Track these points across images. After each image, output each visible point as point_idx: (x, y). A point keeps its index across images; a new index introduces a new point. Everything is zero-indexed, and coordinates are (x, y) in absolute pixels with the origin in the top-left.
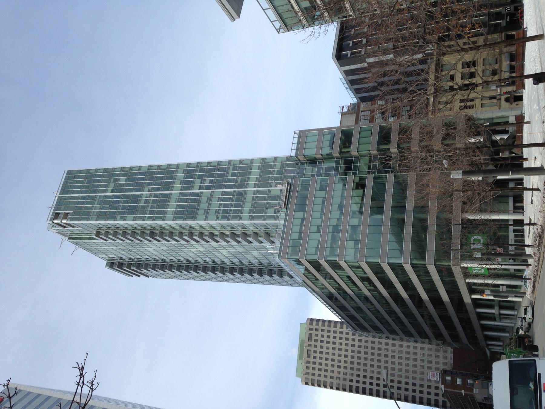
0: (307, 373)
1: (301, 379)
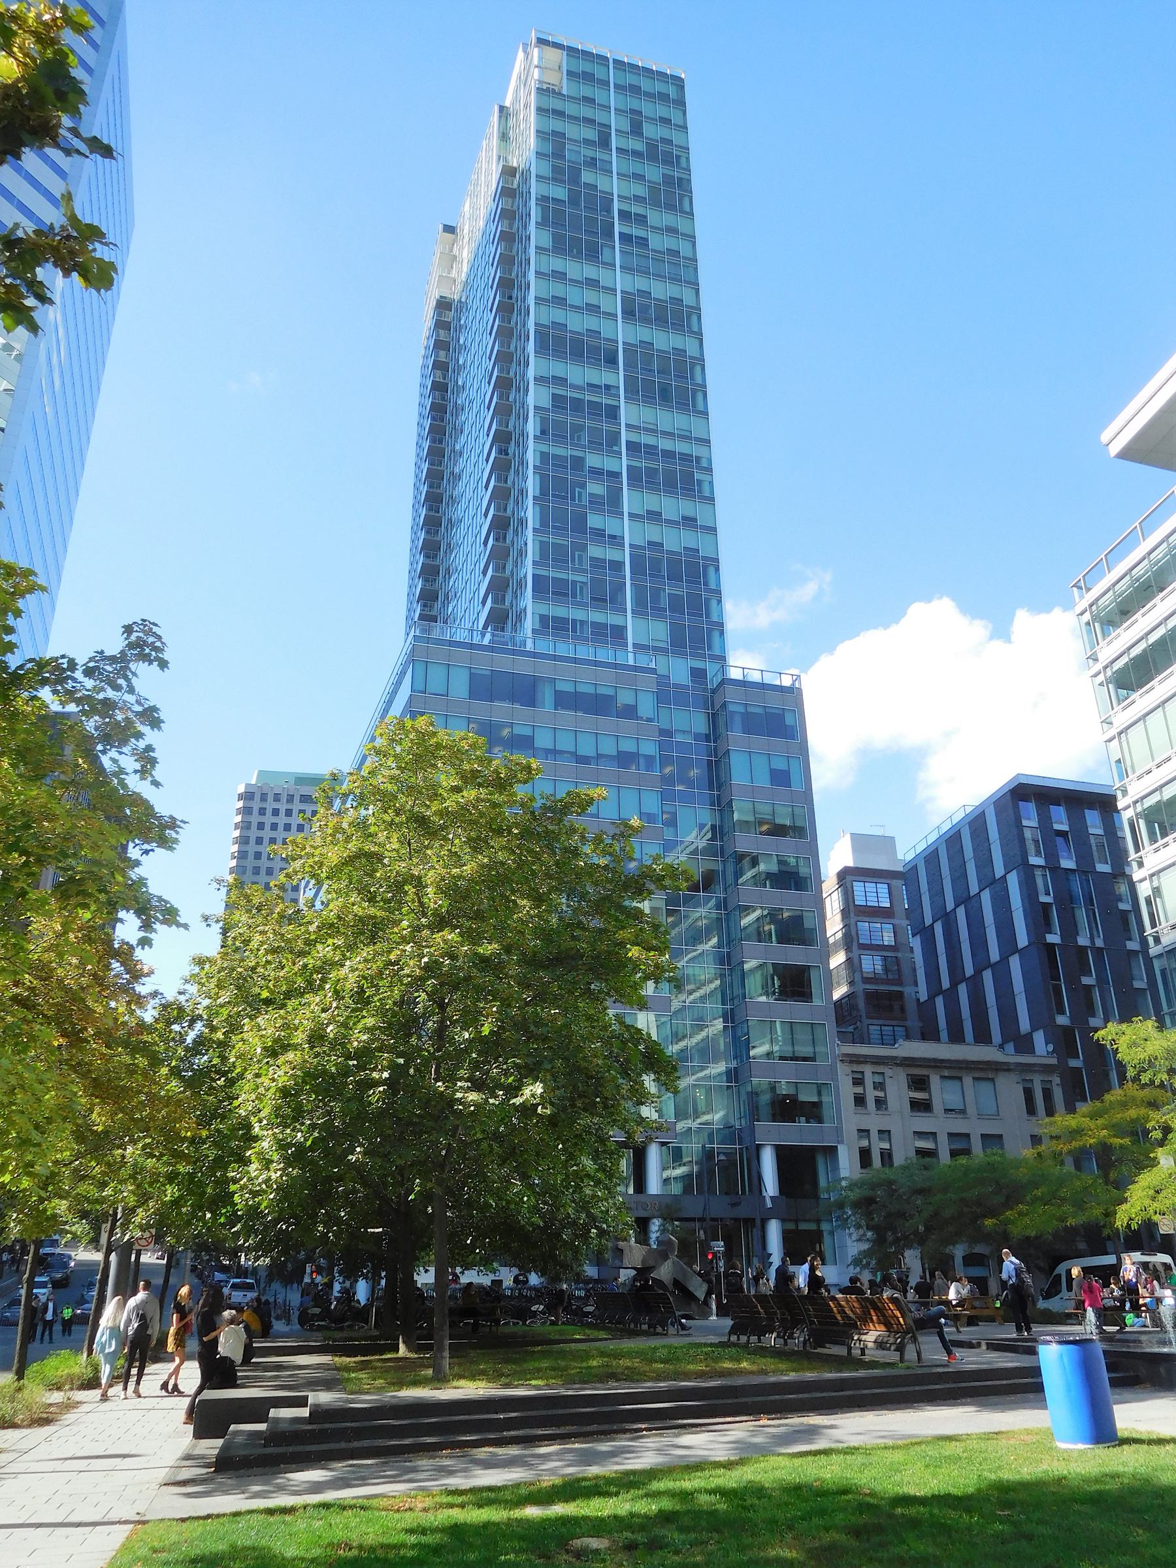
1: (253, 782)
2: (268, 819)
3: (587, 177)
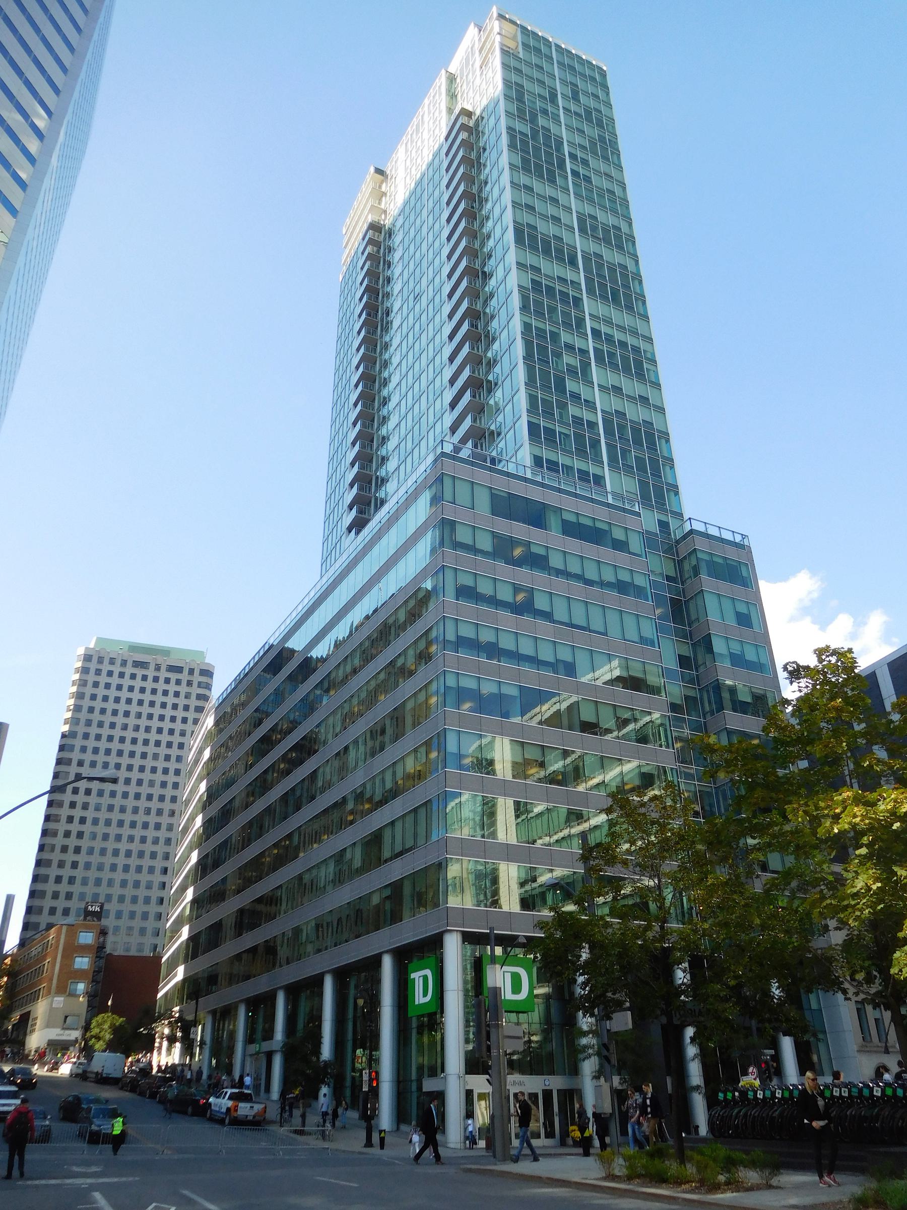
1: (92, 646)
2: (103, 679)
3: (541, 121)
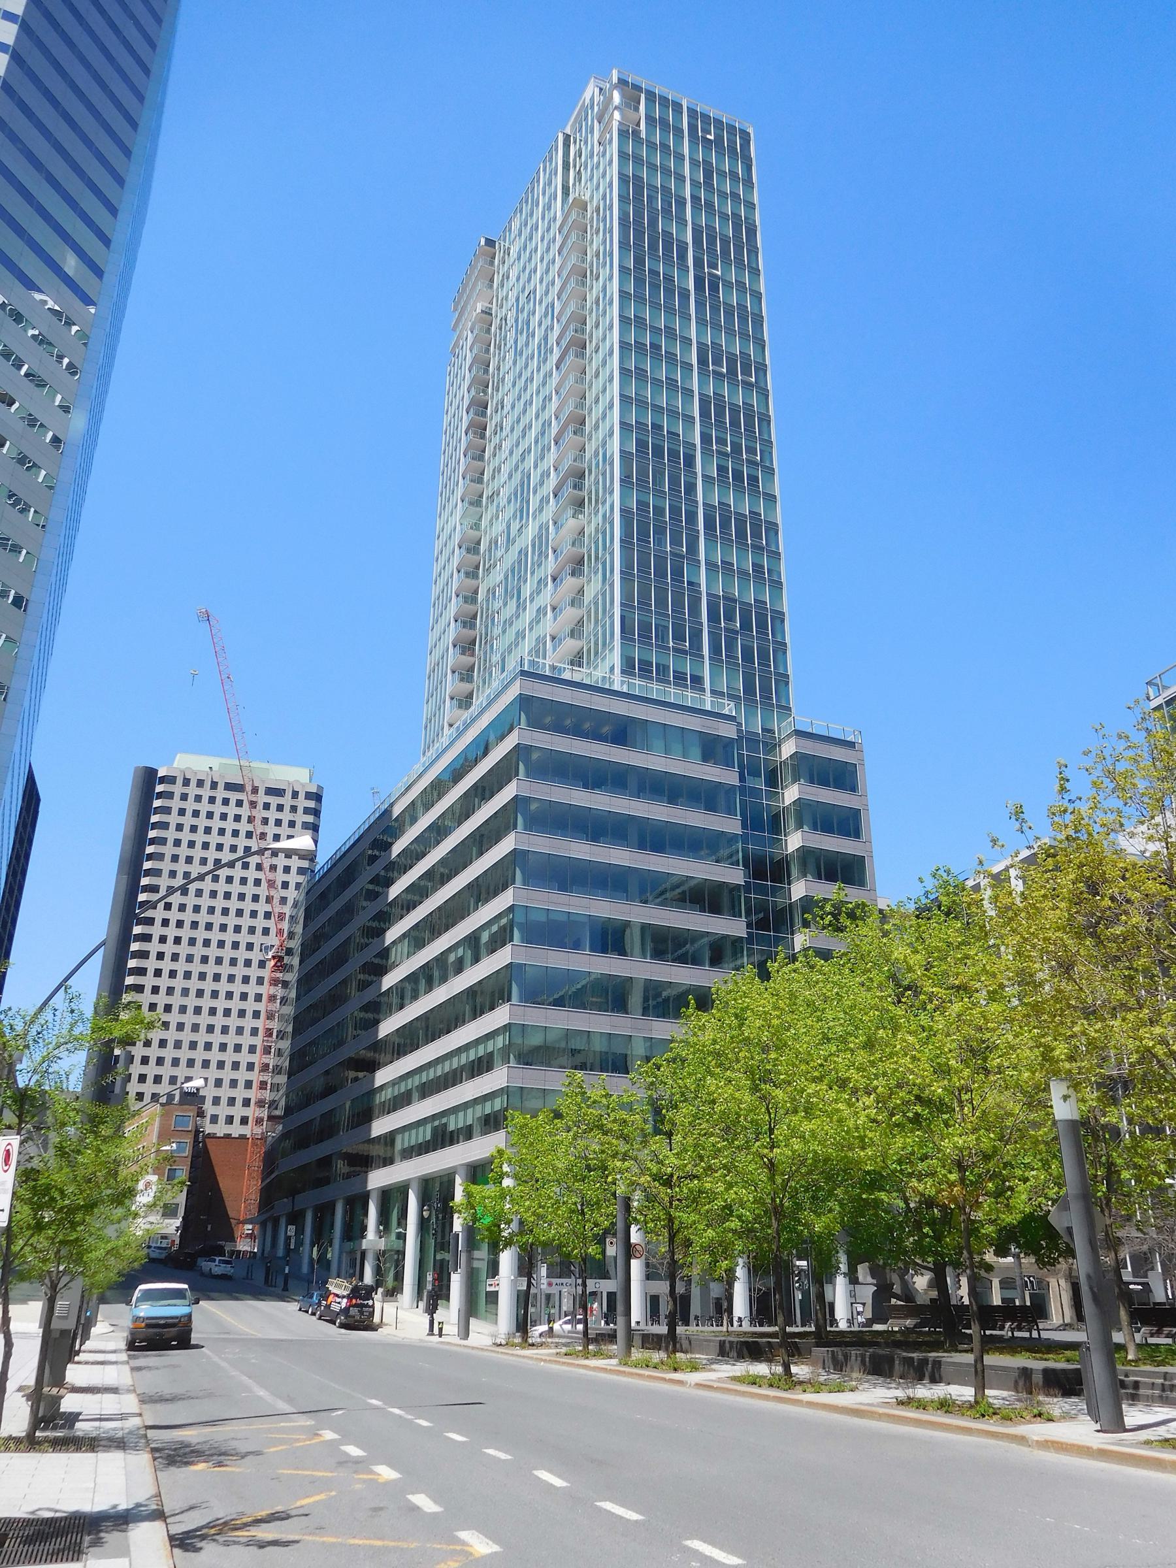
0: (187, 782)
